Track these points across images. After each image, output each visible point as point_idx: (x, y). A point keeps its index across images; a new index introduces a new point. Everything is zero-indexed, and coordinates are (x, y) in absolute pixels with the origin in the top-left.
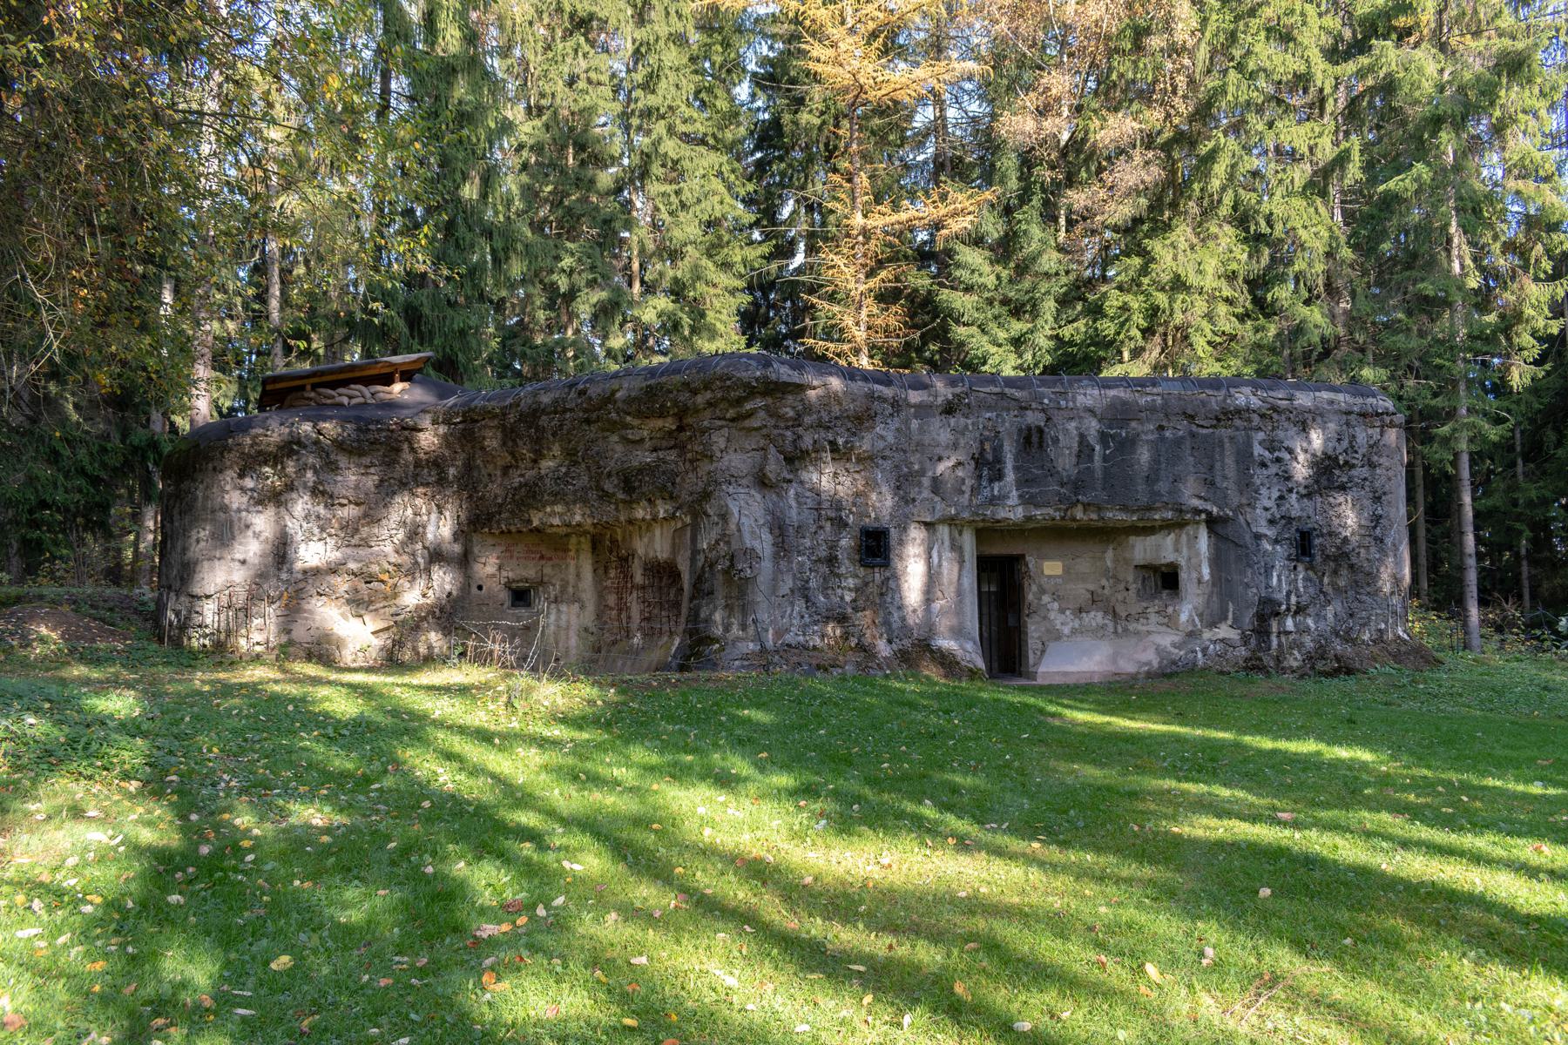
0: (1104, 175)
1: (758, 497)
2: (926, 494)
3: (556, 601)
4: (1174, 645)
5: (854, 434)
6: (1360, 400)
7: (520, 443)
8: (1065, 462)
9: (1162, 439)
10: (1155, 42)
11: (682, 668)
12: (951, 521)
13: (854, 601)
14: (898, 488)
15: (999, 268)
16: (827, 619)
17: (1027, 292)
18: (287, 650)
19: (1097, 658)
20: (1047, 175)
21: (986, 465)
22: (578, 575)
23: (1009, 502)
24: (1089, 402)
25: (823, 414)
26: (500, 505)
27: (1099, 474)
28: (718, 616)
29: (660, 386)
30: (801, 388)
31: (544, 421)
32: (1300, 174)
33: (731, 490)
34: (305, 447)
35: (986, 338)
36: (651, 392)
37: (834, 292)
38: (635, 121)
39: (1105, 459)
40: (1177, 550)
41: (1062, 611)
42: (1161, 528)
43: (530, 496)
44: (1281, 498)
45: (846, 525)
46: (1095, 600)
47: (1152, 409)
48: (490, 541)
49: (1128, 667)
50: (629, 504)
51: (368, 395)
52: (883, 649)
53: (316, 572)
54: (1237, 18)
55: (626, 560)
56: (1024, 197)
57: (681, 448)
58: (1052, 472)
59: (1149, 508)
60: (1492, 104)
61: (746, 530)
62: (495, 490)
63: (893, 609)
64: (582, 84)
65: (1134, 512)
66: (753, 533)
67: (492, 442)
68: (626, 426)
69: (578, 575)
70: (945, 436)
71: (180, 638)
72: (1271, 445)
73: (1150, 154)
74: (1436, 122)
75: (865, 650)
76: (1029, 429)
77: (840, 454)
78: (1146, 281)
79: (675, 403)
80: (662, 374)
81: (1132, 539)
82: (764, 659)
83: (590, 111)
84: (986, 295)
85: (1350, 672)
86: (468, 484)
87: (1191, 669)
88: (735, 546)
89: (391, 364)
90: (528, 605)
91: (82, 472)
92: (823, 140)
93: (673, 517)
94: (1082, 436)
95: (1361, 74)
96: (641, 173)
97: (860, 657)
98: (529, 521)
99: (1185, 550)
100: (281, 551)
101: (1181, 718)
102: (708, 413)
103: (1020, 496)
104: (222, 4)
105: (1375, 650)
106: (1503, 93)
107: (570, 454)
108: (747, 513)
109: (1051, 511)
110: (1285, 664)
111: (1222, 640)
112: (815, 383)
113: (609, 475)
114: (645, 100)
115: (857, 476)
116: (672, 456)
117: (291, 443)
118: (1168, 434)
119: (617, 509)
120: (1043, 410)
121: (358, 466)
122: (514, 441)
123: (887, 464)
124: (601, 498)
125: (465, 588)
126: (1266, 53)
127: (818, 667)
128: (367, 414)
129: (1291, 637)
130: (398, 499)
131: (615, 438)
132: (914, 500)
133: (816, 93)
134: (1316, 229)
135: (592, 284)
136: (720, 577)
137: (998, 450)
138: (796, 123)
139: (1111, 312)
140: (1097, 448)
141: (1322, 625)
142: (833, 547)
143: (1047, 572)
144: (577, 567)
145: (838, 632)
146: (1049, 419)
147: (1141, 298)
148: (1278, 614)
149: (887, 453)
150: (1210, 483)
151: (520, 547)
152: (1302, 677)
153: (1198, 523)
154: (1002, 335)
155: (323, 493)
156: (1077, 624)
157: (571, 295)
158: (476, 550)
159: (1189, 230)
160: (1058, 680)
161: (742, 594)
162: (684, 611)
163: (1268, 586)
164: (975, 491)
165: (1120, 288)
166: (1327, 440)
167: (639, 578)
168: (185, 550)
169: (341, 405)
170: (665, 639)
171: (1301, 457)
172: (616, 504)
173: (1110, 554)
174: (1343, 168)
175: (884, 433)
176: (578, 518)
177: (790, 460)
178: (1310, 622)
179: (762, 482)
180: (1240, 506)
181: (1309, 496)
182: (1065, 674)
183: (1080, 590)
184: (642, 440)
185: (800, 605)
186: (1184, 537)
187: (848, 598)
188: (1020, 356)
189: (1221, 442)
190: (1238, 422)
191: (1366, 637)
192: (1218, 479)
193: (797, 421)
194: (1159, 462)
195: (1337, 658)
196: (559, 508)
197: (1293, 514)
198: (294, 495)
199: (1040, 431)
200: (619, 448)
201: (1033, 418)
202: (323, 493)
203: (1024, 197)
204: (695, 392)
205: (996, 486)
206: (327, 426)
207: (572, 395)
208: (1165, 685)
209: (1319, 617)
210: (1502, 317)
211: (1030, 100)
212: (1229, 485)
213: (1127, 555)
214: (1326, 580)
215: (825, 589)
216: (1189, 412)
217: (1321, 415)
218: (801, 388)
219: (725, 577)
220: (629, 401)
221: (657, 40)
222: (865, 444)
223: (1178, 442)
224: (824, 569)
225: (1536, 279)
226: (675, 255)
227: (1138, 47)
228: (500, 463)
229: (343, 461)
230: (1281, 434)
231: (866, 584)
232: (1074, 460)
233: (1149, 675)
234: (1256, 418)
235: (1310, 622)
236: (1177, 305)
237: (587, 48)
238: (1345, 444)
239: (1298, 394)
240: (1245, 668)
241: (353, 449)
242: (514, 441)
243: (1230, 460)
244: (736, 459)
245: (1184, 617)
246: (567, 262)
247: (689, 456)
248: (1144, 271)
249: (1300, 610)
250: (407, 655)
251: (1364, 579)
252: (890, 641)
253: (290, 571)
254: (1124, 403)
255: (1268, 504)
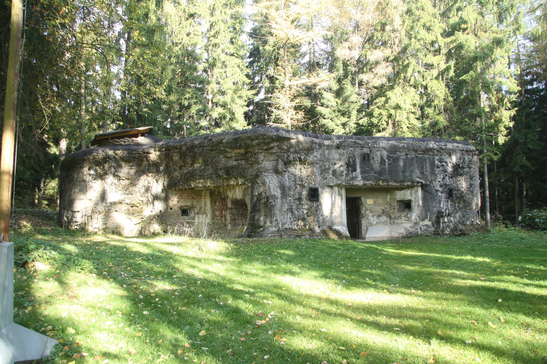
0: (373, 70)
1: (275, 177)
2: (331, 176)
3: (197, 214)
4: (410, 227)
5: (307, 155)
6: (466, 146)
7: (187, 158)
8: (376, 165)
9: (407, 158)
10: (388, 28)
11: (249, 236)
12: (339, 186)
13: (307, 213)
14: (321, 174)
15: (337, 100)
16: (299, 219)
17: (347, 108)
18: (106, 230)
19: (385, 232)
20: (353, 69)
21: (351, 166)
22: (205, 205)
23: (358, 179)
24: (384, 145)
25: (297, 148)
26: (179, 180)
27: (387, 170)
28: (262, 219)
29: (239, 138)
30: (289, 139)
31: (196, 150)
32: (435, 72)
33: (266, 174)
34: (111, 159)
35: (333, 123)
36: (236, 140)
37: (279, 107)
38: (210, 48)
39: (389, 164)
40: (411, 195)
41: (373, 216)
42: (406, 188)
43: (191, 176)
44: (444, 178)
45: (305, 187)
46: (384, 212)
47: (403, 148)
48: (175, 192)
49: (395, 235)
50: (228, 179)
51: (130, 141)
52: (317, 230)
53: (115, 203)
54: (413, 22)
55: (224, 199)
56: (346, 76)
57: (247, 160)
58: (372, 169)
59: (403, 181)
60: (492, 54)
61: (272, 188)
62: (177, 174)
63: (320, 216)
64: (192, 35)
65: (398, 182)
66: (274, 189)
67: (176, 158)
68: (226, 152)
69: (205, 205)
70: (337, 156)
71: (68, 226)
72: (441, 161)
73: (388, 64)
74: (475, 59)
75: (311, 230)
76: (364, 154)
77: (302, 162)
78: (387, 105)
79: (245, 144)
80: (240, 134)
81: (396, 192)
82: (280, 233)
83: (195, 45)
84: (333, 109)
85: (465, 235)
86: (168, 172)
87: (417, 235)
88: (268, 194)
89: (138, 130)
90: (187, 215)
91: (33, 168)
92: (274, 55)
93: (244, 184)
94: (382, 157)
95: (452, 42)
96: (212, 66)
97: (310, 232)
98: (191, 186)
99: (414, 195)
100: (103, 197)
101: (420, 250)
102: (257, 148)
103: (362, 177)
104: (383, 1)
105: (471, 227)
106: (495, 50)
107: (205, 162)
108: (272, 183)
109: (372, 182)
110: (445, 233)
111: (426, 225)
112: (294, 137)
113: (221, 169)
114: (214, 41)
115: (308, 170)
116: (243, 162)
117: (106, 158)
118: (409, 156)
119: (223, 181)
120: (369, 148)
121: (129, 166)
122: (185, 157)
123: (318, 166)
124: (217, 177)
125: (166, 209)
126: (423, 33)
127: (297, 236)
128: (132, 147)
129: (447, 224)
130: (142, 178)
131: (222, 156)
132: (326, 178)
133: (271, 40)
134: (440, 90)
135: (195, 103)
136: (263, 205)
137: (354, 161)
138: (265, 50)
139: (376, 115)
140: (387, 161)
141: (455, 220)
142: (300, 194)
143: (368, 203)
144: (205, 202)
145: (302, 224)
146: (371, 151)
147: (386, 111)
148: (443, 216)
149: (318, 162)
150: (422, 173)
151: (185, 195)
152: (450, 237)
153: (418, 186)
154: (339, 122)
155: (117, 176)
156: (378, 220)
157: (189, 107)
158: (170, 195)
159: (400, 89)
160: (372, 240)
161: (270, 211)
162: (249, 217)
163: (440, 207)
164: (347, 175)
165: (378, 107)
166: (457, 159)
167: (230, 205)
168: (70, 195)
169: (121, 145)
170: (240, 227)
171: (449, 165)
172: (223, 179)
173: (388, 197)
174: (448, 71)
175: (316, 155)
176: (209, 184)
177: (285, 164)
178: (452, 219)
179: (276, 171)
180: (432, 180)
181: (451, 177)
182: (375, 237)
183: (379, 209)
184: (232, 157)
185: (290, 214)
186: (413, 191)
187: (305, 212)
188: (345, 129)
189: (425, 159)
190: (430, 153)
191: (468, 223)
192: (425, 172)
193: (288, 151)
194: (406, 166)
195: (461, 230)
196: (201, 181)
197: (448, 183)
198: (107, 176)
199: (368, 155)
200: (223, 159)
201: (366, 150)
202: (117, 176)
203: (346, 76)
204: (252, 140)
205: (354, 173)
206: (118, 152)
207: (206, 141)
208: (410, 240)
209: (455, 217)
210: (495, 121)
211: (346, 44)
212: (428, 174)
213: (394, 197)
214: (456, 205)
215: (297, 209)
216: (415, 149)
217: (455, 151)
218: (289, 139)
219: (264, 204)
220: (228, 143)
221: (218, 21)
222: (310, 159)
223: (412, 159)
224: (297, 202)
225: (506, 109)
226: (223, 93)
227: (383, 30)
228: (178, 165)
229: (123, 164)
230: (443, 157)
231: (311, 207)
232: (379, 165)
233: (403, 237)
234: (436, 151)
235: (452, 219)
236: (398, 114)
237: (193, 23)
238: (462, 160)
239: (448, 144)
240: (434, 234)
241: (127, 160)
242: (185, 157)
243: (428, 166)
244: (268, 164)
245: (413, 218)
246: (187, 96)
247: (250, 162)
248: (386, 102)
249: (449, 215)
250: (147, 233)
251: (468, 205)
252: (319, 227)
253: (106, 203)
254: (395, 146)
255: (440, 180)
